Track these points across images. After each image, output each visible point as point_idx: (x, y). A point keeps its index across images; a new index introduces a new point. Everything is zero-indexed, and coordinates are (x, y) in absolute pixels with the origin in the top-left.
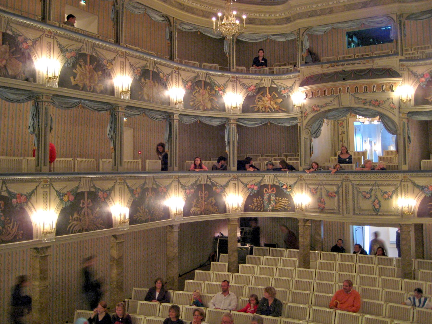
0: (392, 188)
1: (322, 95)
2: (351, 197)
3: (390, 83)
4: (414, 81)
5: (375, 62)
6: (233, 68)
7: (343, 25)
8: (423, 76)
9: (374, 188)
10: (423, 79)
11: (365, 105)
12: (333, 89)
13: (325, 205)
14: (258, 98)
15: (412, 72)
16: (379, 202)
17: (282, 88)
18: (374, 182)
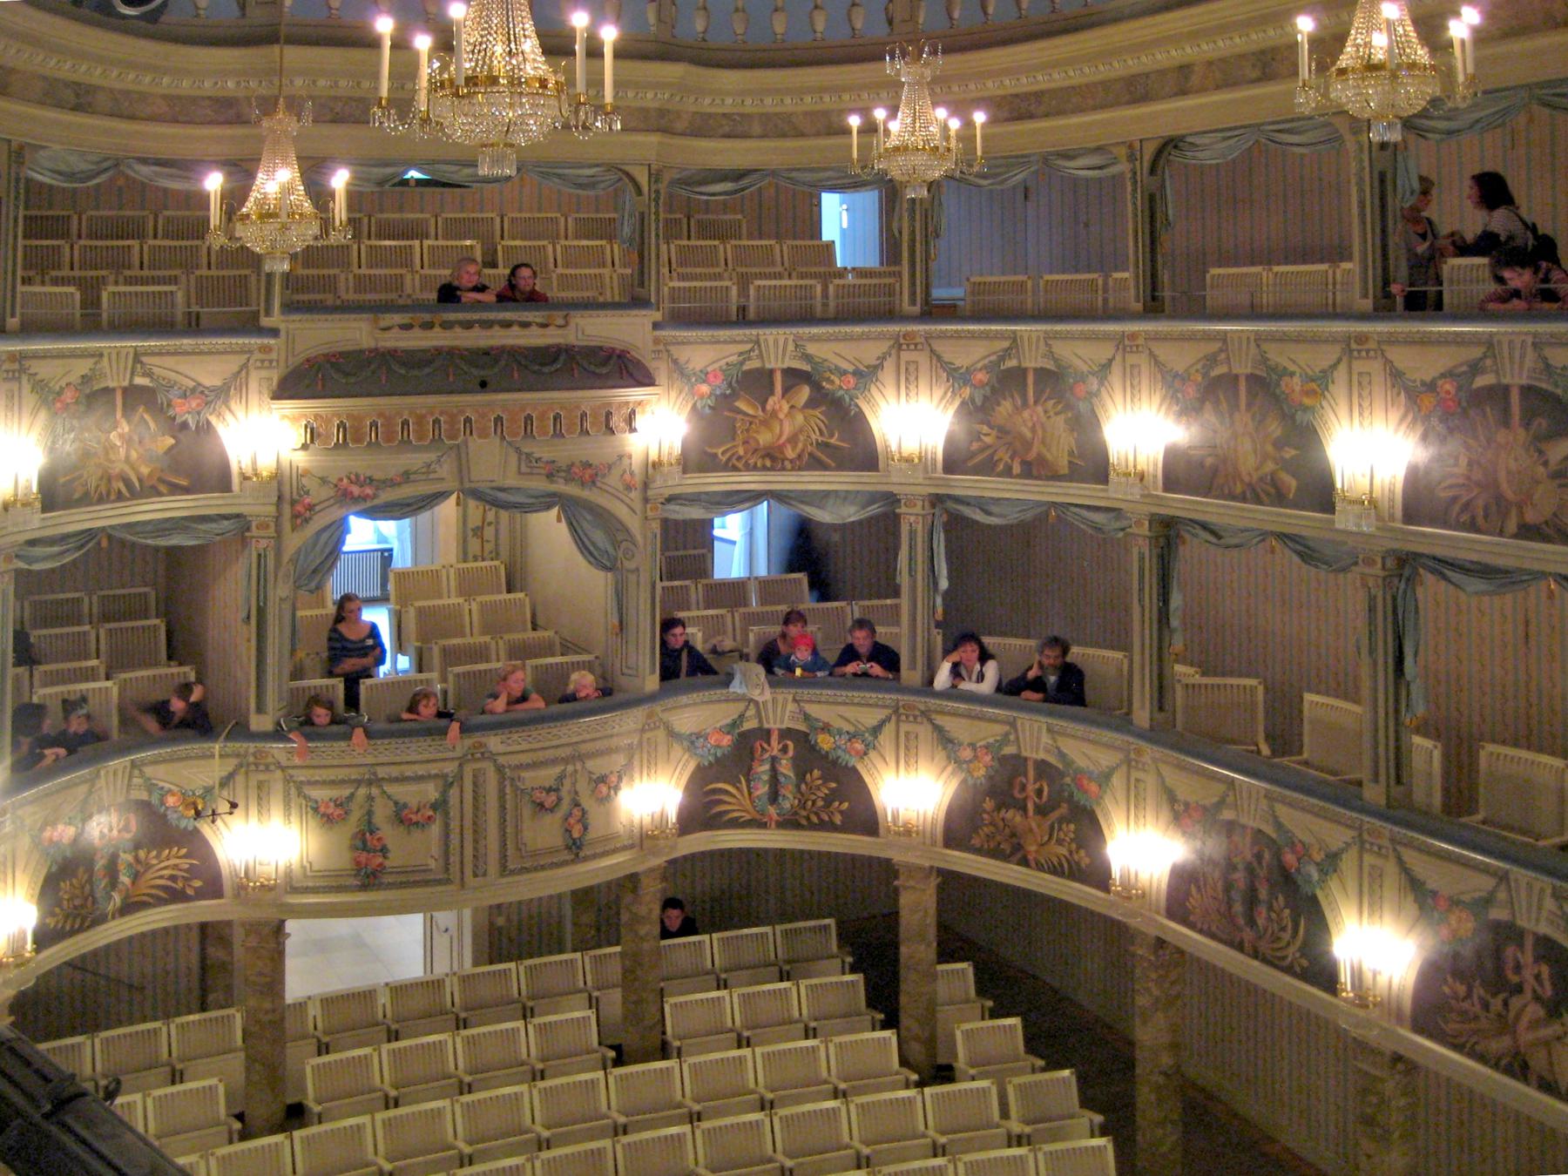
1: (389, 439)
5: (573, 322)
6: (13, 315)
8: (704, 376)
10: (705, 388)
11: (552, 482)
13: (385, 857)
15: (675, 362)
16: (584, 812)
17: (175, 391)
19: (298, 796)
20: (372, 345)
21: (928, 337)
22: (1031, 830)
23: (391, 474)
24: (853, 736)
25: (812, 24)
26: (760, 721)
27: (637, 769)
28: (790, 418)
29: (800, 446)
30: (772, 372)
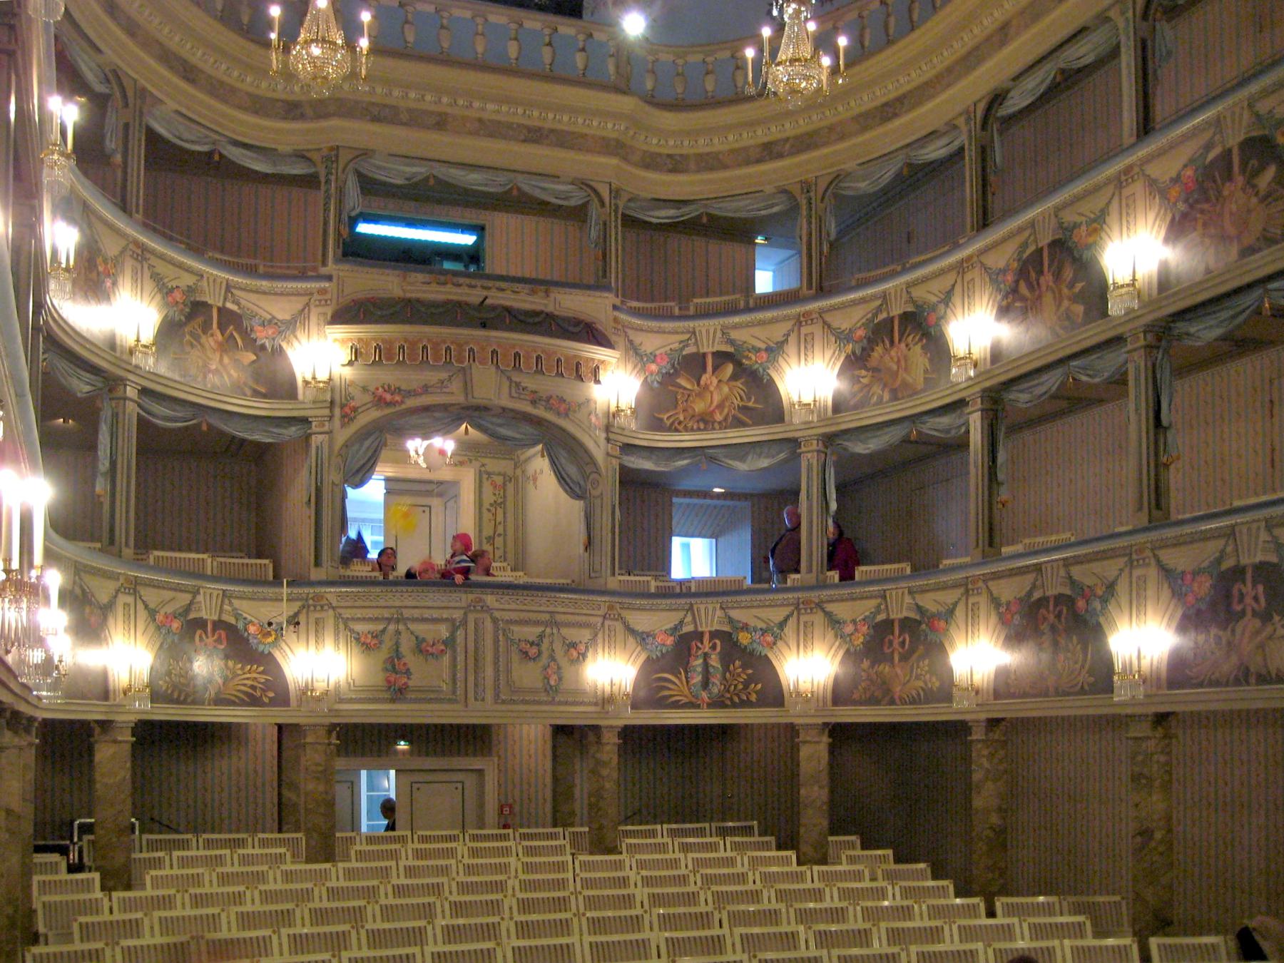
0: (586, 634)
2: (489, 657)
3: (593, 360)
4: (635, 367)
5: (552, 296)
7: (462, 173)
8: (653, 358)
9: (548, 630)
10: (654, 367)
12: (448, 349)
14: (191, 334)
15: (631, 342)
16: (559, 668)
18: (547, 616)
19: (346, 629)
20: (401, 294)
21: (821, 312)
22: (897, 675)
23: (414, 386)
24: (764, 632)
25: (734, 80)
26: (696, 626)
27: (600, 646)
28: (719, 389)
29: (726, 411)
30: (704, 355)
